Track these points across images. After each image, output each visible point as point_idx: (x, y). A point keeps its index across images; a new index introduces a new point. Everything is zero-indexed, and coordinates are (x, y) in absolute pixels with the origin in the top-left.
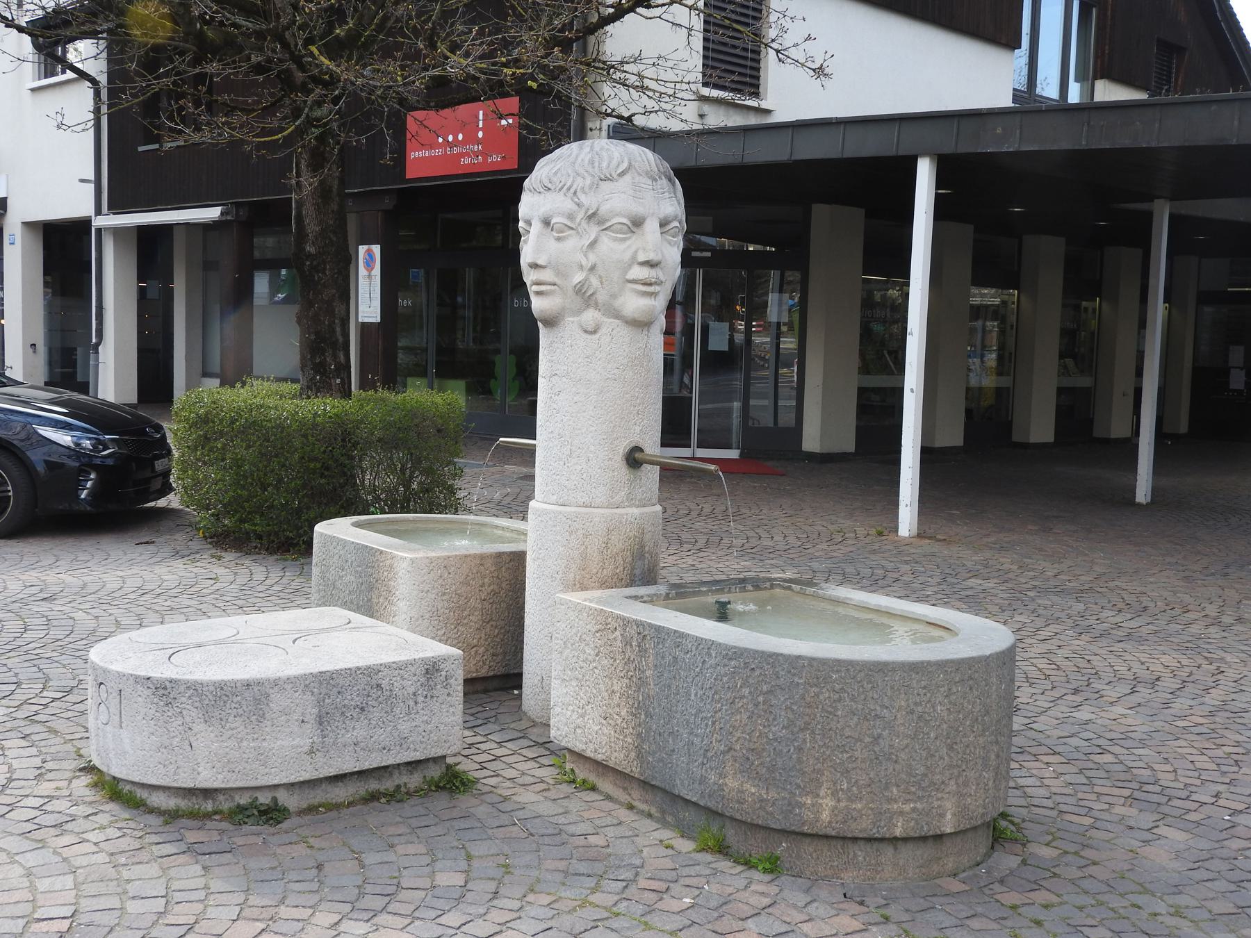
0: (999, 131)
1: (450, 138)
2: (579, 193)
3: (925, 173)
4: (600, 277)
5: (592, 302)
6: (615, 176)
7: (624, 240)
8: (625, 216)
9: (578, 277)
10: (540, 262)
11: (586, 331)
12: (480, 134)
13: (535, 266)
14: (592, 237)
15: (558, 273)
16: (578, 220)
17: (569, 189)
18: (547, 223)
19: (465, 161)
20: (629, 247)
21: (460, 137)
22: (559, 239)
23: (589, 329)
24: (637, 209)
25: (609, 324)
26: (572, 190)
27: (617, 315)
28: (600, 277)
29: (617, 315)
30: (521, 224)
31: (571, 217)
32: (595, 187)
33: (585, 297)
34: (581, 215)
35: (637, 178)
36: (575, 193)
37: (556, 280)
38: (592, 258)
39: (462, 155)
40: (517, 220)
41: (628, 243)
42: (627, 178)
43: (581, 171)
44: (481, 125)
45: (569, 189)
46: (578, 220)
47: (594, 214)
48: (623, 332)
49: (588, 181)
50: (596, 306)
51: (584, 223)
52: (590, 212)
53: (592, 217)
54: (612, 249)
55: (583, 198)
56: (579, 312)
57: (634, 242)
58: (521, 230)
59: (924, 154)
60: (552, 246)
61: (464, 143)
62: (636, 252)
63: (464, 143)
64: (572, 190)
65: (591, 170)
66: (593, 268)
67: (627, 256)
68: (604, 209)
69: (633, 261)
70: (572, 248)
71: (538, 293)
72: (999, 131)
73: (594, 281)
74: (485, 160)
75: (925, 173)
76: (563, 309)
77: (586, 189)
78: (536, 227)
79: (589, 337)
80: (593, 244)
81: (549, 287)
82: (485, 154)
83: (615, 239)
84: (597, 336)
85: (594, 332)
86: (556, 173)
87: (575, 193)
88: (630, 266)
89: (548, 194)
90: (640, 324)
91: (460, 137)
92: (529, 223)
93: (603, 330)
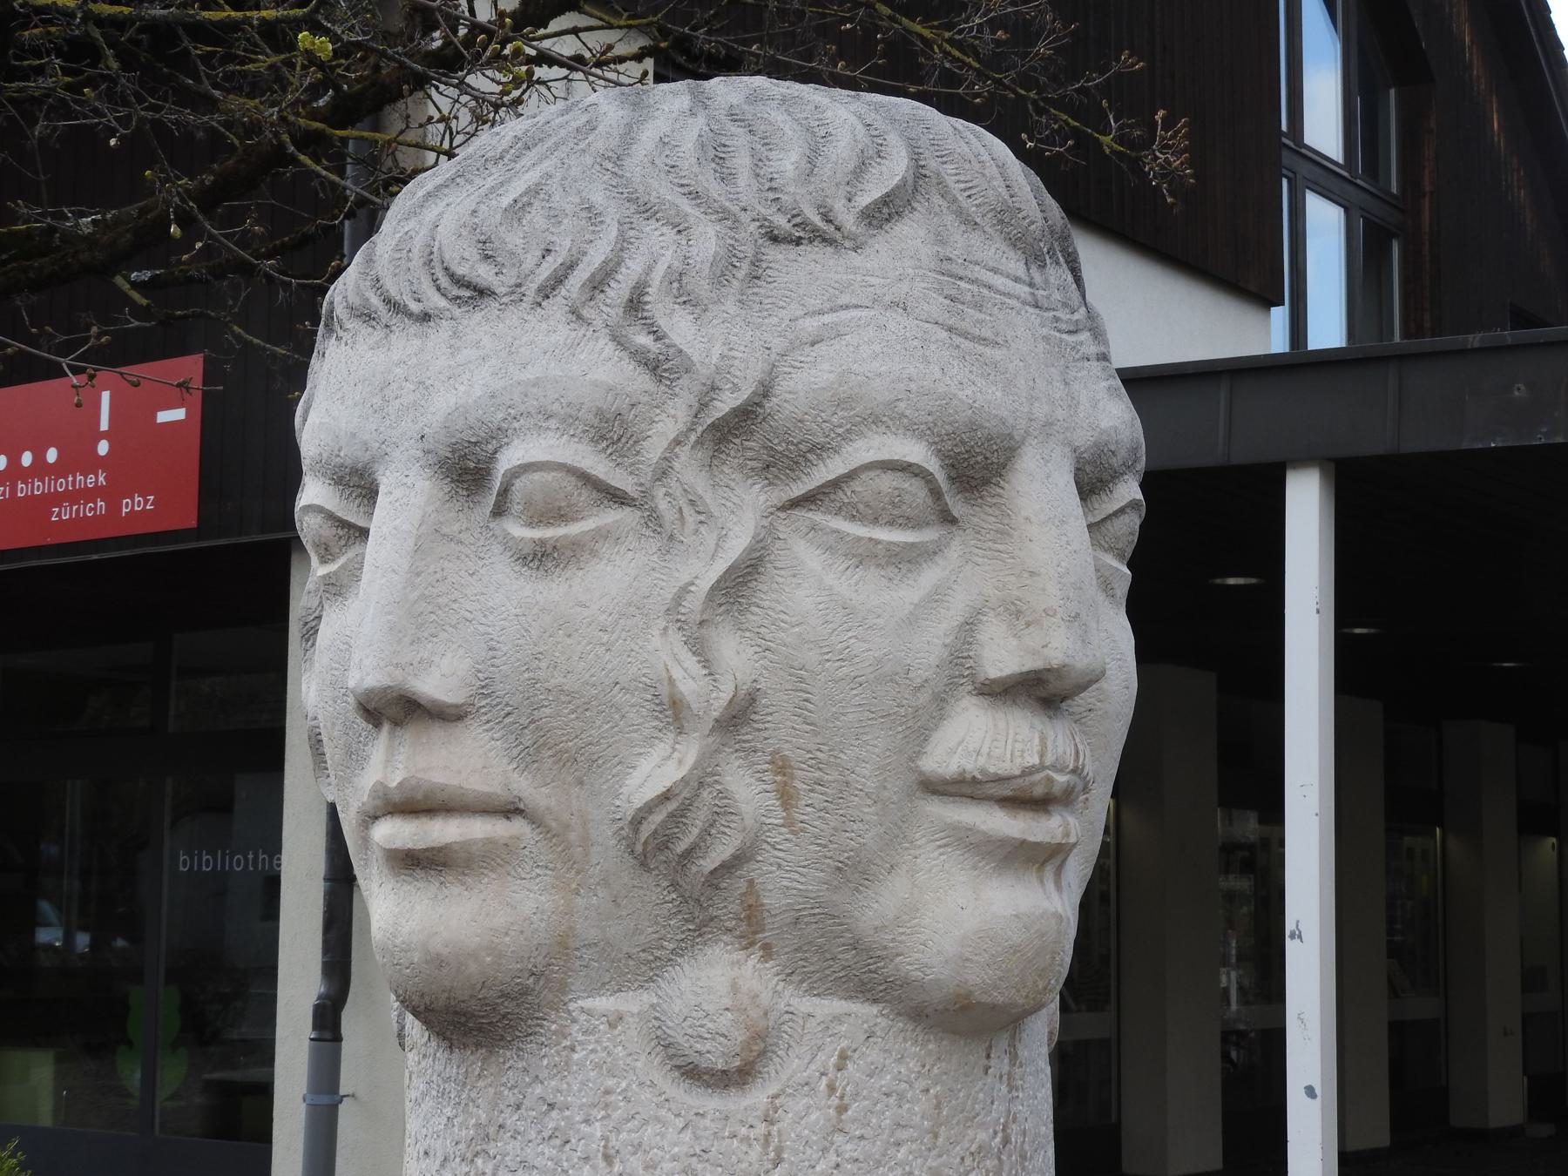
0: (1520, 392)
1: (27, 459)
2: (659, 306)
3: (1306, 507)
4: (781, 766)
5: (728, 907)
6: (848, 219)
7: (904, 560)
8: (912, 429)
9: (655, 770)
10: (432, 686)
11: (693, 1073)
12: (103, 448)
13: (393, 710)
14: (737, 546)
15: (536, 743)
16: (654, 449)
17: (597, 285)
18: (466, 470)
19: (64, 513)
20: (937, 597)
21: (52, 455)
22: (540, 558)
23: (716, 1056)
24: (980, 392)
25: (827, 1020)
26: (618, 291)
27: (865, 974)
28: (781, 766)
29: (865, 974)
30: (313, 493)
31: (612, 431)
32: (742, 272)
33: (686, 876)
34: (669, 422)
35: (960, 241)
36: (635, 304)
37: (524, 786)
38: (737, 657)
39: (56, 499)
40: (289, 474)
41: (930, 576)
42: (910, 232)
43: (663, 190)
44: (104, 425)
45: (597, 285)
46: (654, 449)
47: (746, 417)
48: (894, 1068)
49: (707, 241)
50: (752, 929)
51: (689, 470)
52: (726, 403)
53: (738, 431)
54: (843, 604)
55: (681, 328)
56: (648, 965)
57: (959, 575)
58: (308, 527)
59: (1302, 462)
60: (501, 599)
61: (59, 470)
62: (969, 627)
63: (59, 470)
64: (618, 291)
65: (715, 189)
66: (738, 717)
67: (928, 648)
68: (804, 387)
69: (963, 678)
70: (616, 603)
71: (412, 862)
72: (1520, 392)
73: (747, 790)
74: (114, 507)
75: (1306, 507)
76: (563, 946)
77: (701, 285)
78: (406, 499)
79: (712, 1102)
80: (739, 584)
81: (478, 829)
82: (112, 494)
83: (866, 556)
84: (757, 1097)
85: (736, 1077)
86: (517, 210)
87: (635, 304)
88: (941, 703)
89: (479, 325)
90: (962, 1021)
91: (52, 455)
92: (360, 484)
93: (790, 1066)
